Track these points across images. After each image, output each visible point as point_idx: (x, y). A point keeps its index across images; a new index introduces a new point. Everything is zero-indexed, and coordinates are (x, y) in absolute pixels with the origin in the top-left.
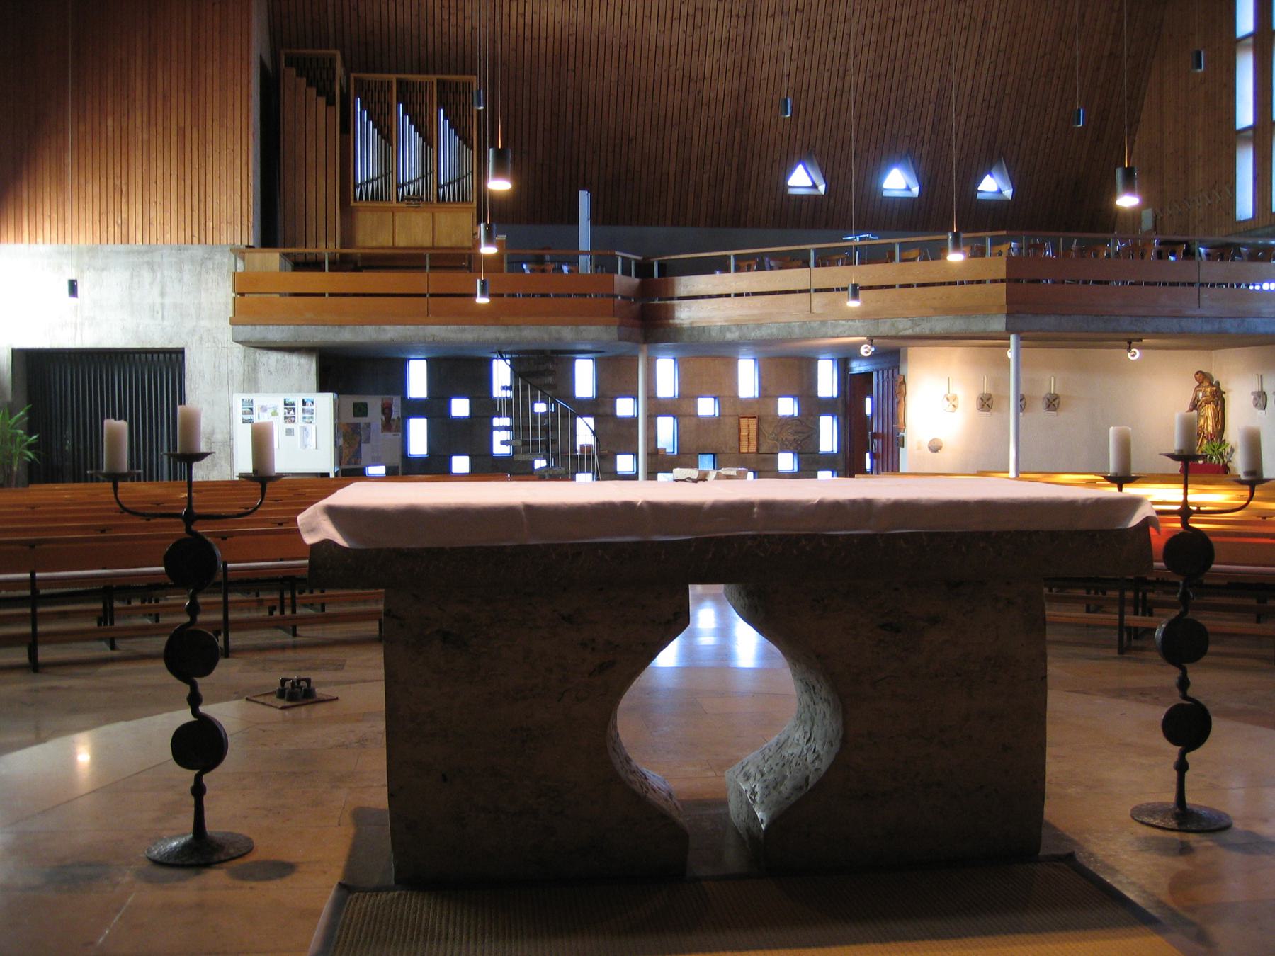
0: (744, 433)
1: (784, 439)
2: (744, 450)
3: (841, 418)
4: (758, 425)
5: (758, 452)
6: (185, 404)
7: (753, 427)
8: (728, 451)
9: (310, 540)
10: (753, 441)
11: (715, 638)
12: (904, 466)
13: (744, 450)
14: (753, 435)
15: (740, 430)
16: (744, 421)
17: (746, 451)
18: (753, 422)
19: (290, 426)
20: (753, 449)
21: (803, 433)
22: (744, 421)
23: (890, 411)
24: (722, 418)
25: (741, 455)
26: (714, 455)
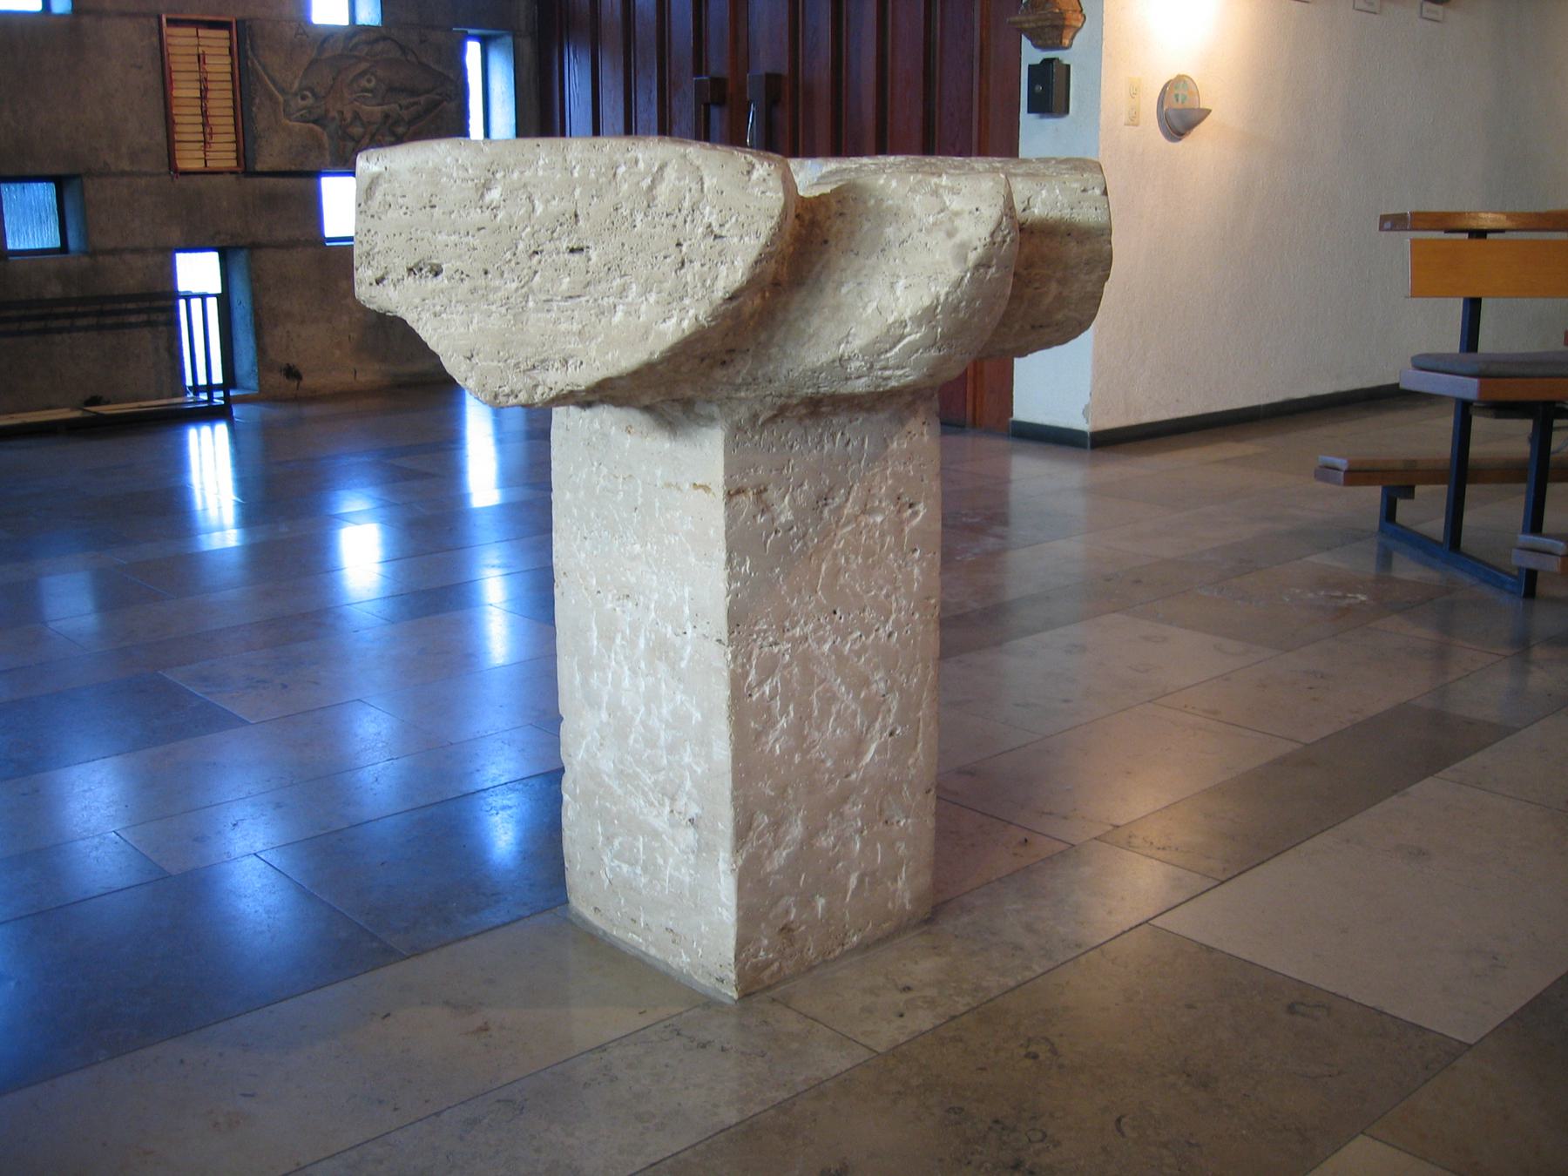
0: (185, 90)
1: (349, 116)
2: (190, 159)
3: (527, 46)
4: (241, 53)
5: (246, 167)
6: (351, 239)
7: (220, 65)
8: (125, 166)
9: (792, 517)
10: (223, 121)
11: (206, 548)
12: (1102, 219)
13: (190, 159)
14: (221, 102)
15: (165, 83)
16: (181, 41)
17: (199, 165)
18: (217, 43)
19: (375, 283)
20: (224, 155)
21: (413, 92)
22: (181, 41)
23: (906, 61)
24: (86, 21)
25: (182, 181)
26: (60, 182)
